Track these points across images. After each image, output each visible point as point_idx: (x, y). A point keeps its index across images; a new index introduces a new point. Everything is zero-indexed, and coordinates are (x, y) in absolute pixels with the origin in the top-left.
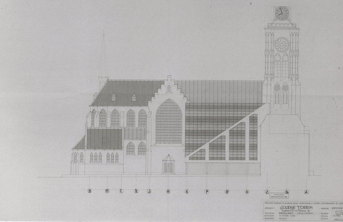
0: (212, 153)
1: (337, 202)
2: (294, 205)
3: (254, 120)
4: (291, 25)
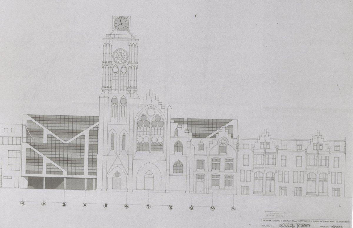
0: (91, 168)
1: (337, 221)
2: (293, 223)
3: (94, 134)
4: (129, 37)
